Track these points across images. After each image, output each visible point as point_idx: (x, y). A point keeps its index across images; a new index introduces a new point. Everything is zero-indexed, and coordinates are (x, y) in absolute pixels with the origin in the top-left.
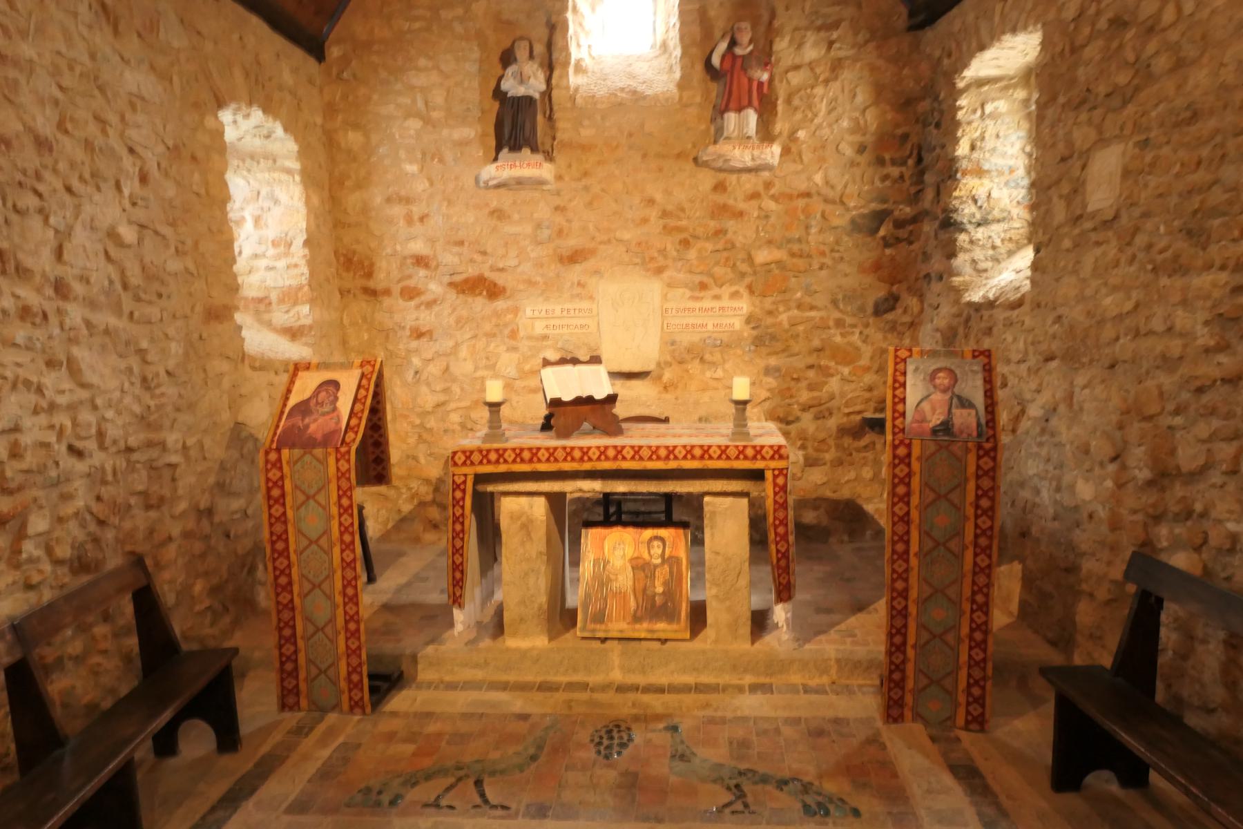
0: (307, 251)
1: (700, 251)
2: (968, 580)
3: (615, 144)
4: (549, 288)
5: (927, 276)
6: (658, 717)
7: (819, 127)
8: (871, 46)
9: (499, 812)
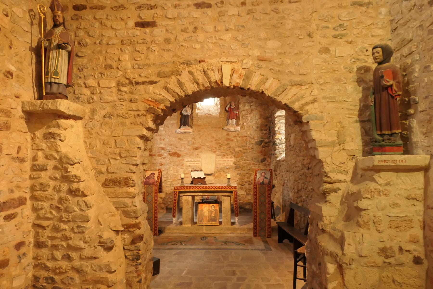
1: (223, 148)
2: (267, 210)
4: (191, 155)
5: (272, 154)
7: (249, 123)
8: (259, 107)
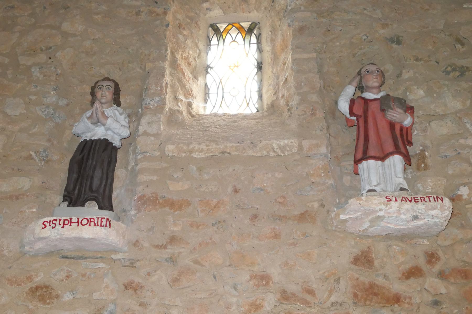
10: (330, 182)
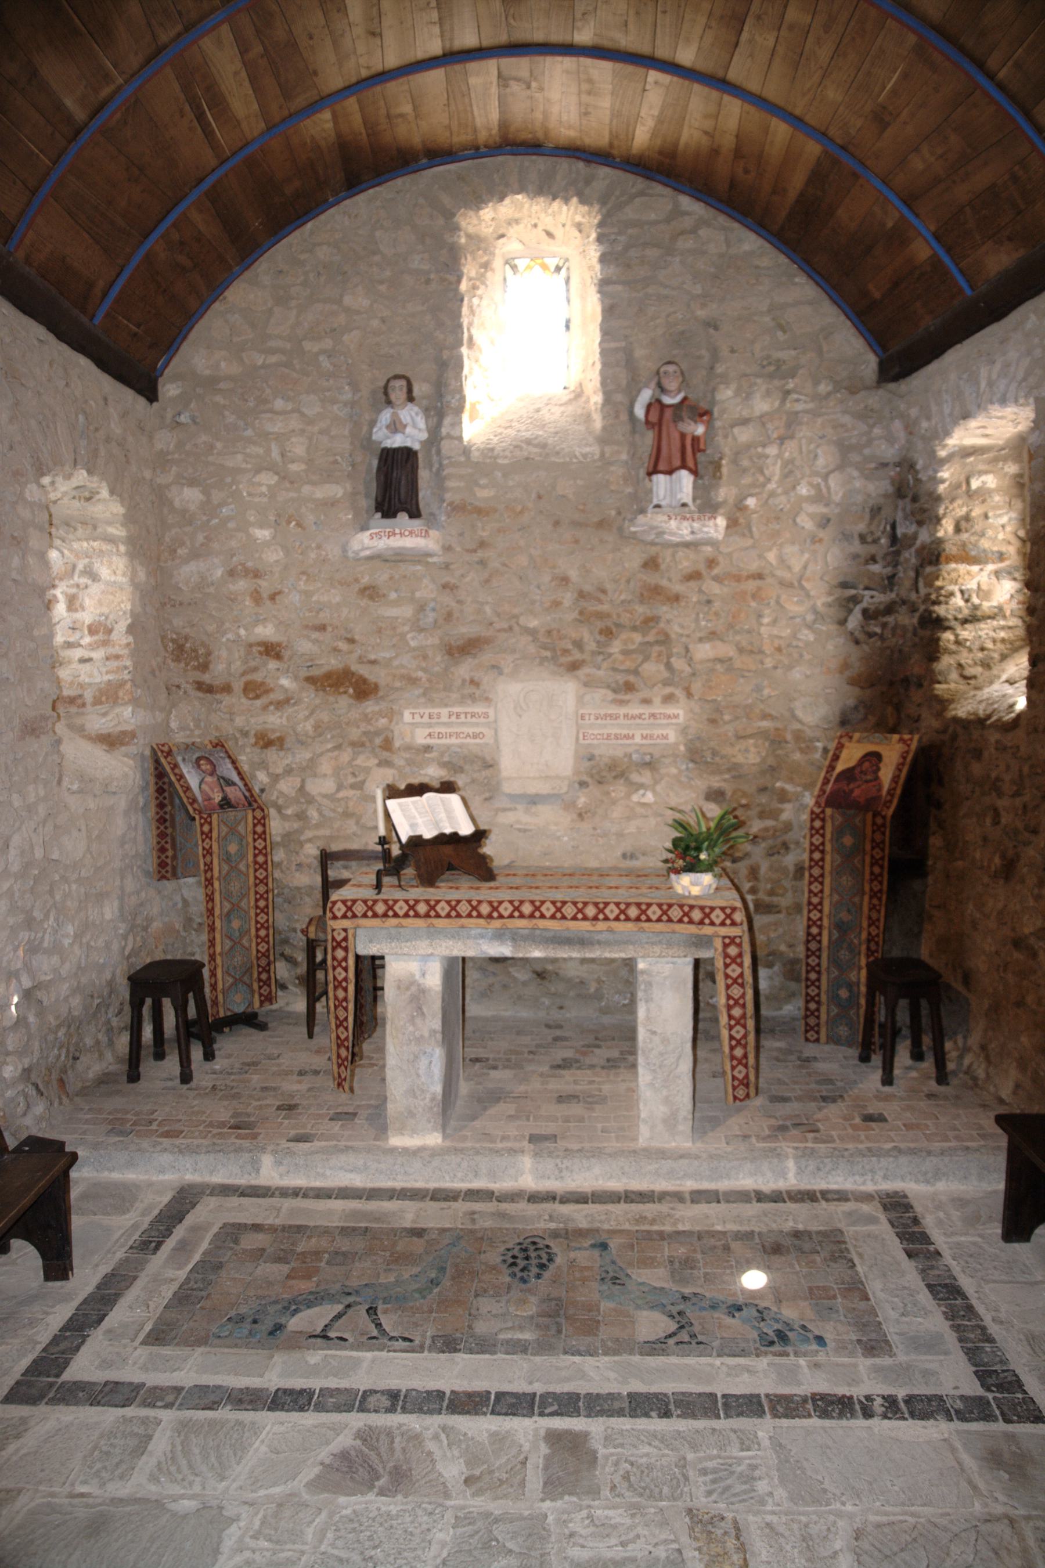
0: (131, 639)
3: (519, 508)
6: (581, 1233)
9: (401, 1344)
10: (629, 490)
